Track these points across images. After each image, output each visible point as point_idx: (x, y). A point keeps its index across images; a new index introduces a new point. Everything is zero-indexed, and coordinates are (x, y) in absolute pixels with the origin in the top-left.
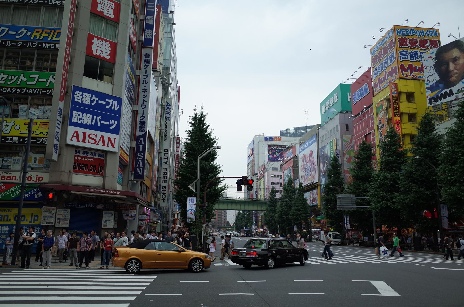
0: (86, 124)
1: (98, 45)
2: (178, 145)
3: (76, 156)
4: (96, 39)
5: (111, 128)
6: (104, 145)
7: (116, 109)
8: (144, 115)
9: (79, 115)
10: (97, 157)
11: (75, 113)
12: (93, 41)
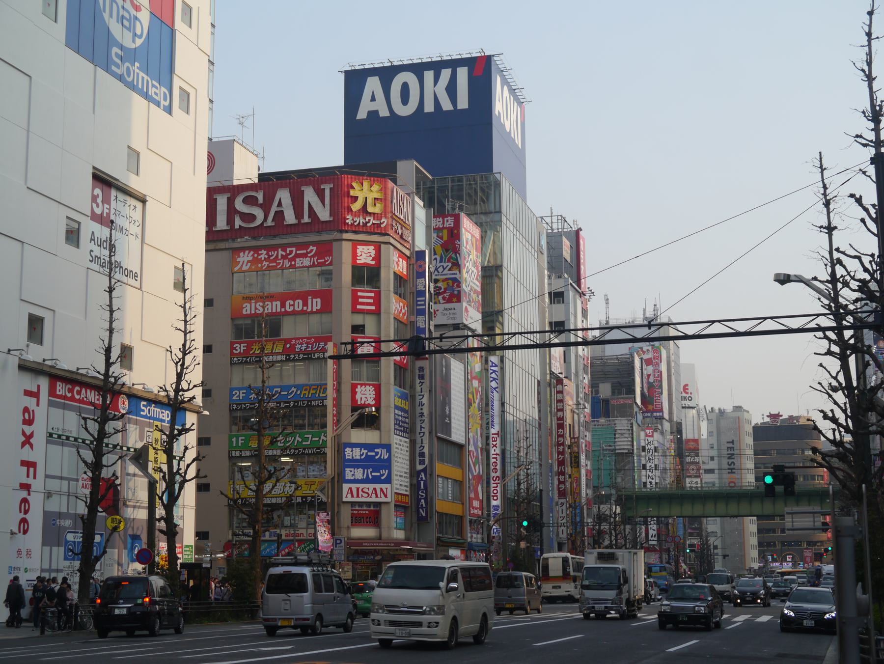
1: (363, 393)
2: (560, 396)
3: (352, 510)
4: (359, 386)
5: (383, 478)
6: (377, 496)
7: (386, 457)
8: (423, 445)
9: (351, 471)
10: (372, 508)
11: (347, 470)
12: (357, 390)
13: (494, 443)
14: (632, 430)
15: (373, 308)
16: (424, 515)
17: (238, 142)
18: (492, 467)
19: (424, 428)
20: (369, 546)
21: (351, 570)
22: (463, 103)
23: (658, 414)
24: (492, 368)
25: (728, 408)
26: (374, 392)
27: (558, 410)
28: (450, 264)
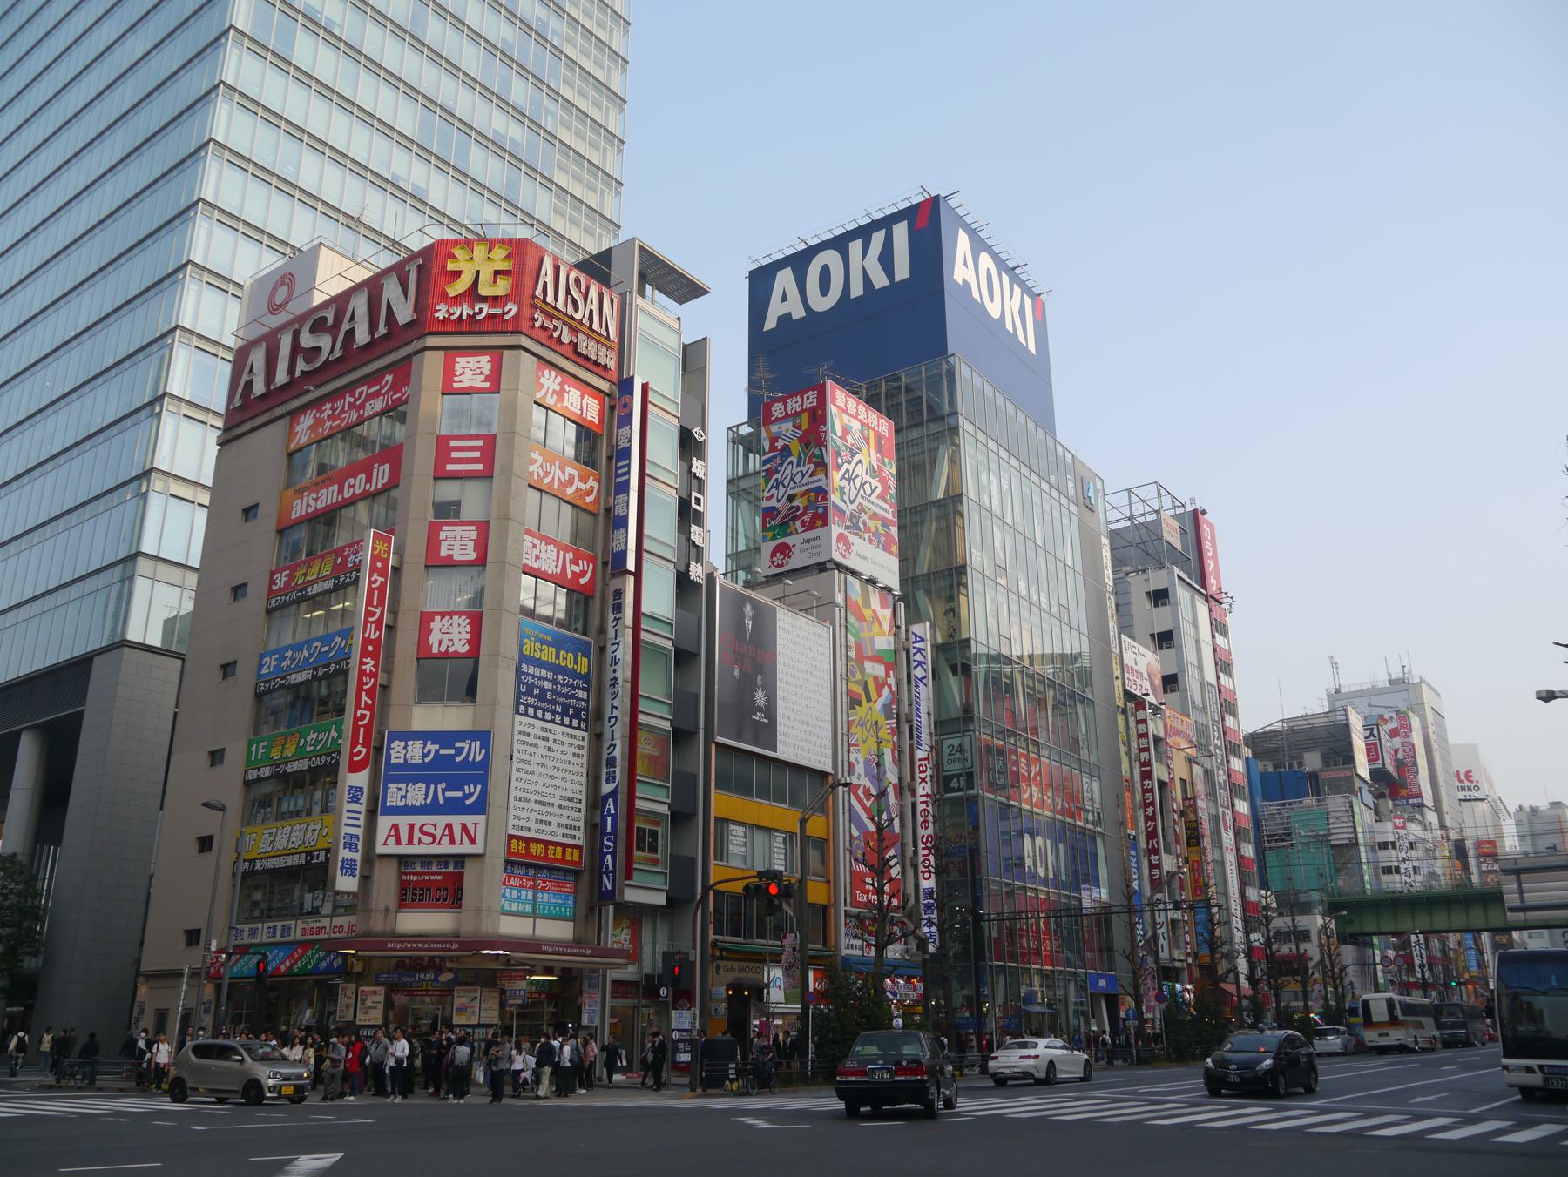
0: (413, 806)
1: (444, 630)
4: (437, 618)
5: (468, 802)
6: (452, 842)
7: (478, 758)
9: (400, 789)
10: (451, 869)
11: (392, 787)
12: (432, 625)
13: (923, 775)
14: (1352, 811)
15: (480, 467)
16: (609, 887)
17: (326, 247)
18: (920, 820)
19: (617, 708)
20: (401, 950)
21: (381, 1006)
22: (902, 271)
23: (1415, 801)
24: (916, 645)
25: (1543, 804)
26: (468, 629)
27: (1141, 750)
28: (812, 466)
